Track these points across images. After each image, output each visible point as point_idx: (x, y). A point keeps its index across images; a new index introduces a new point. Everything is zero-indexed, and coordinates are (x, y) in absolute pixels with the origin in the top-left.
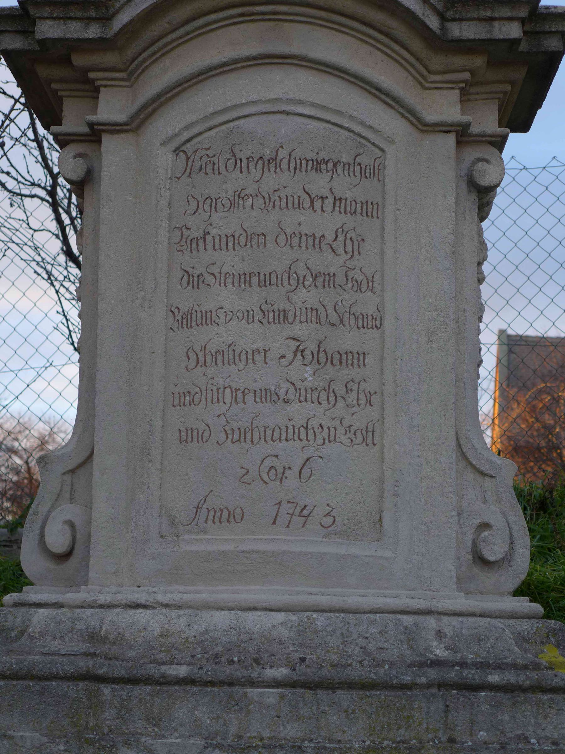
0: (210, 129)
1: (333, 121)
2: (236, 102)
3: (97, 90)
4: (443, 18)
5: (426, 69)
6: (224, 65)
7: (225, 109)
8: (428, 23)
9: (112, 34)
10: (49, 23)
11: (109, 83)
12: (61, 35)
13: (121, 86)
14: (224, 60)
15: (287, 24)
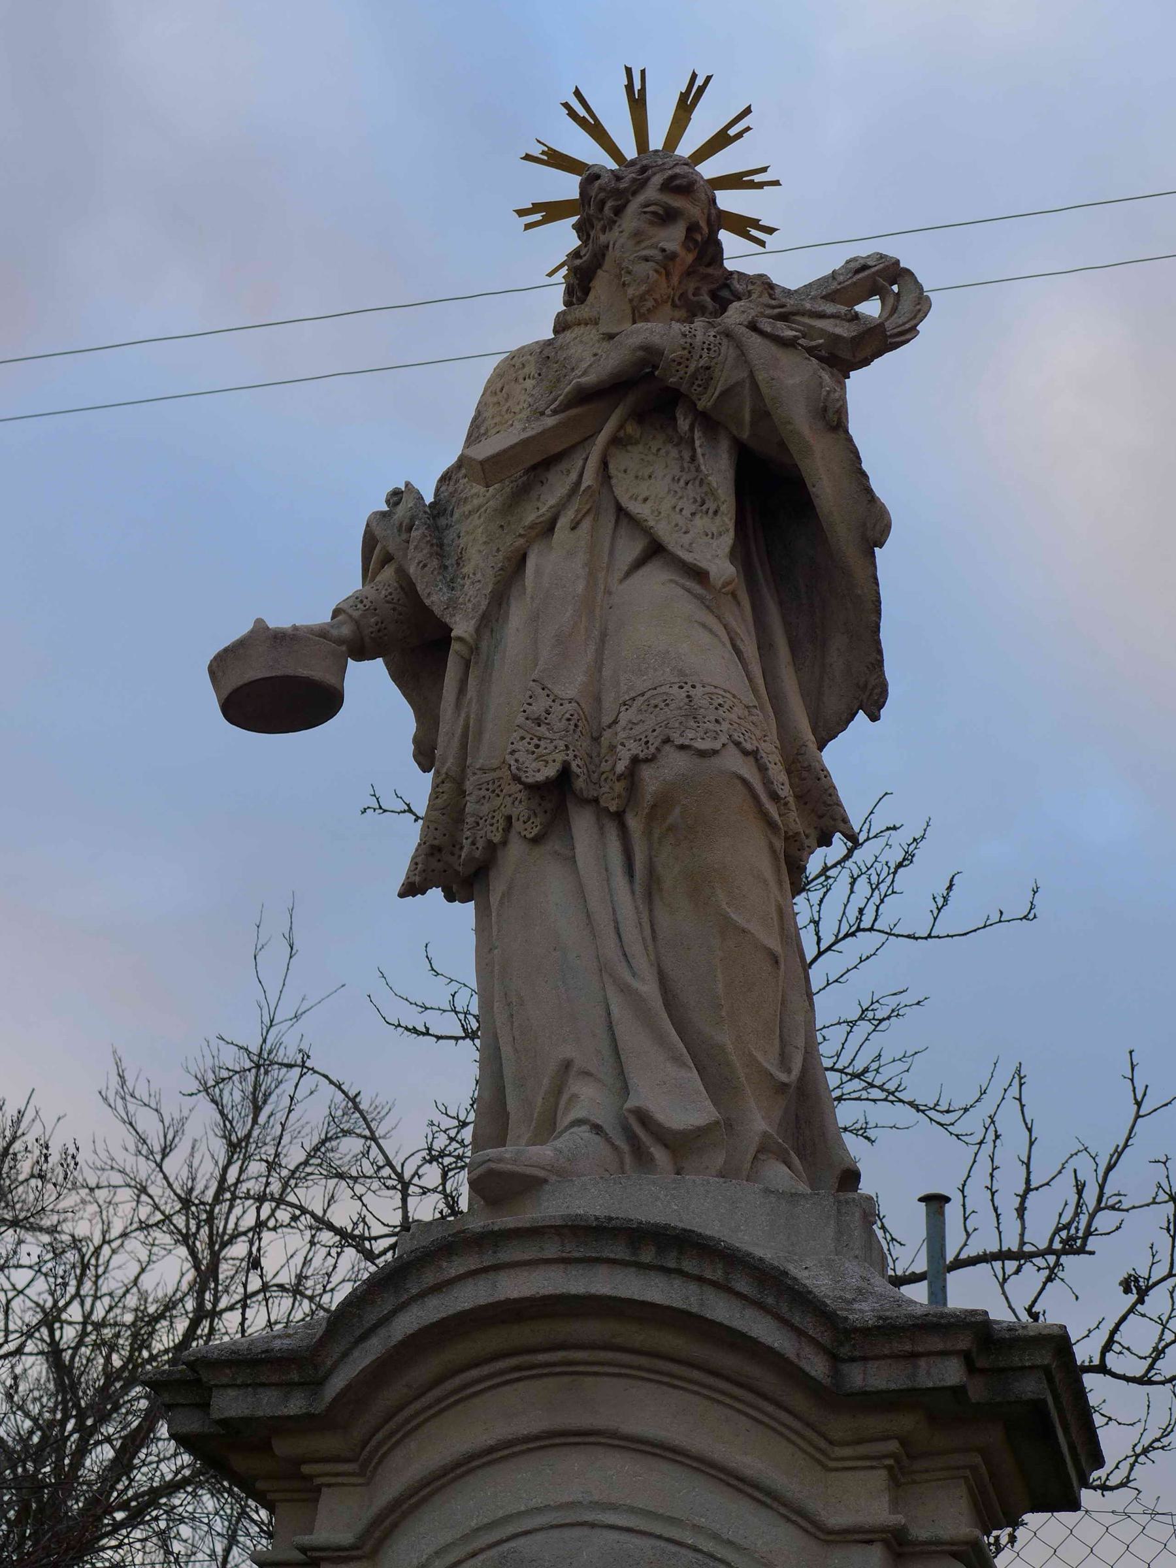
0: (474, 1555)
1: (666, 1535)
2: (511, 1509)
3: (318, 1490)
4: (834, 1358)
5: (826, 1439)
6: (491, 1450)
7: (493, 1522)
8: (807, 1368)
9: (323, 1407)
10: (232, 1393)
11: (333, 1480)
12: (247, 1412)
13: (354, 1485)
14: (491, 1442)
15: (590, 1379)
